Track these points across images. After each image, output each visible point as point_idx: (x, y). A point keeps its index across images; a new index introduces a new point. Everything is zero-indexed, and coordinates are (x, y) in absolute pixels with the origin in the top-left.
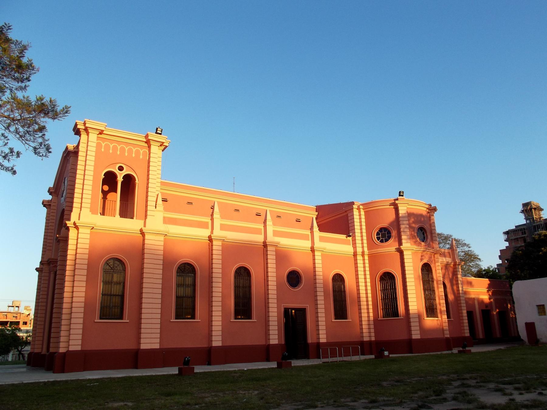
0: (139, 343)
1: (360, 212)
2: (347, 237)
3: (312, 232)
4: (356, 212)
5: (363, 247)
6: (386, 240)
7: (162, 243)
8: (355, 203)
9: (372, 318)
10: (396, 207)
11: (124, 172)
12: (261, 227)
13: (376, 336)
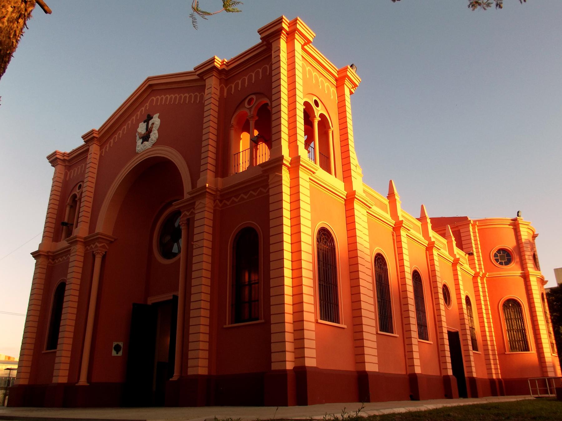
0: (269, 362)
10: (514, 228)
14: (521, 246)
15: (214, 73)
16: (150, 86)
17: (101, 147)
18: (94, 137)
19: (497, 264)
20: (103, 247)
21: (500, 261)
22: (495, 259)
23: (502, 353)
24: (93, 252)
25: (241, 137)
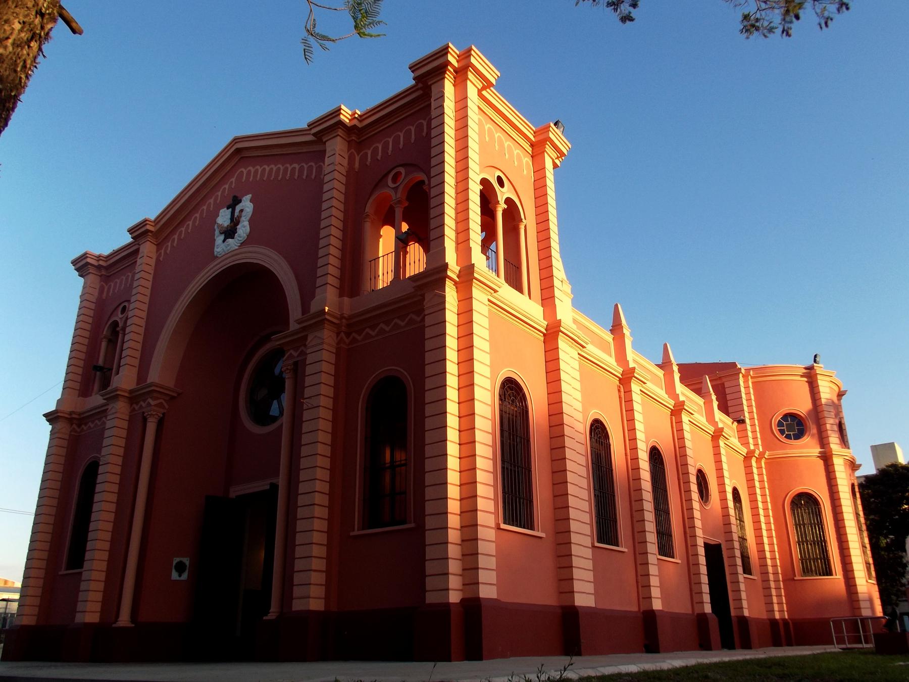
10: (810, 380)
14: (819, 409)
15: (340, 132)
16: (238, 151)
17: (159, 246)
18: (148, 231)
19: (782, 438)
20: (160, 405)
22: (779, 429)
23: (789, 580)
24: (144, 413)
25: (381, 234)
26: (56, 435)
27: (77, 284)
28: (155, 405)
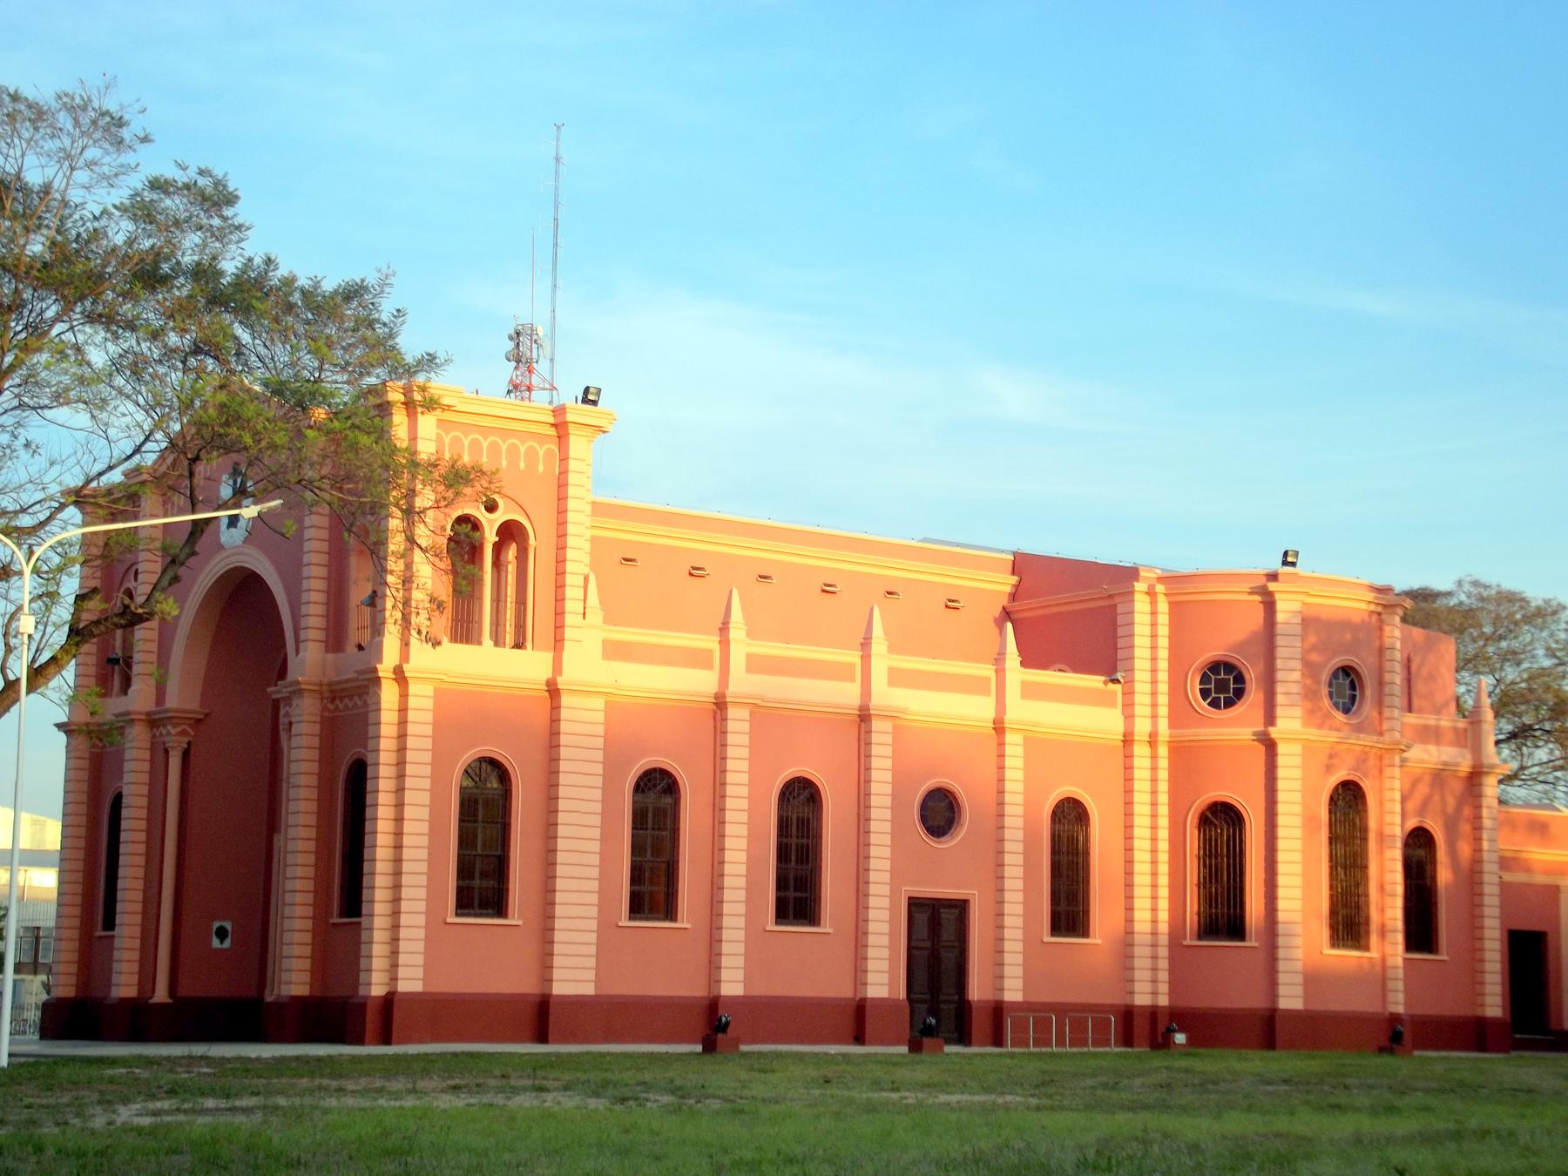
1: (1153, 603)
2: (1105, 683)
3: (1000, 672)
4: (1141, 604)
5: (1154, 717)
6: (1229, 703)
7: (600, 717)
8: (1142, 574)
9: (1164, 927)
10: (1266, 599)
11: (500, 517)
12: (854, 657)
13: (1171, 993)
20: (184, 733)
21: (1213, 695)
24: (164, 744)
26: (73, 754)
27: (62, 738)
28: (177, 735)
